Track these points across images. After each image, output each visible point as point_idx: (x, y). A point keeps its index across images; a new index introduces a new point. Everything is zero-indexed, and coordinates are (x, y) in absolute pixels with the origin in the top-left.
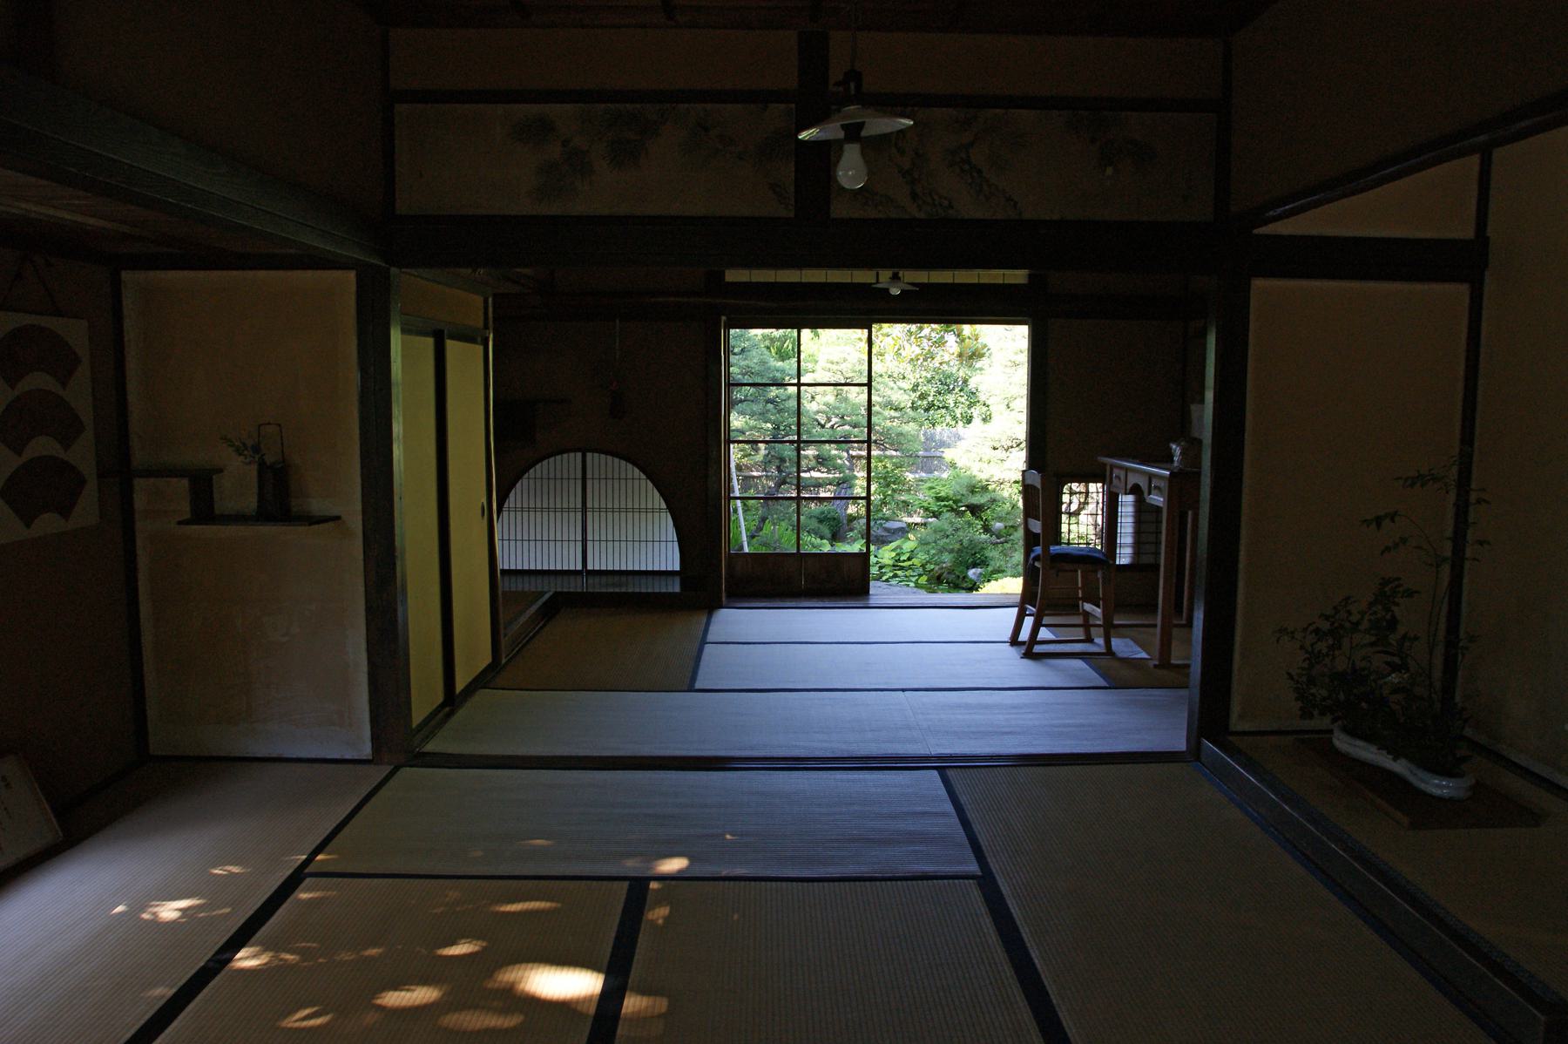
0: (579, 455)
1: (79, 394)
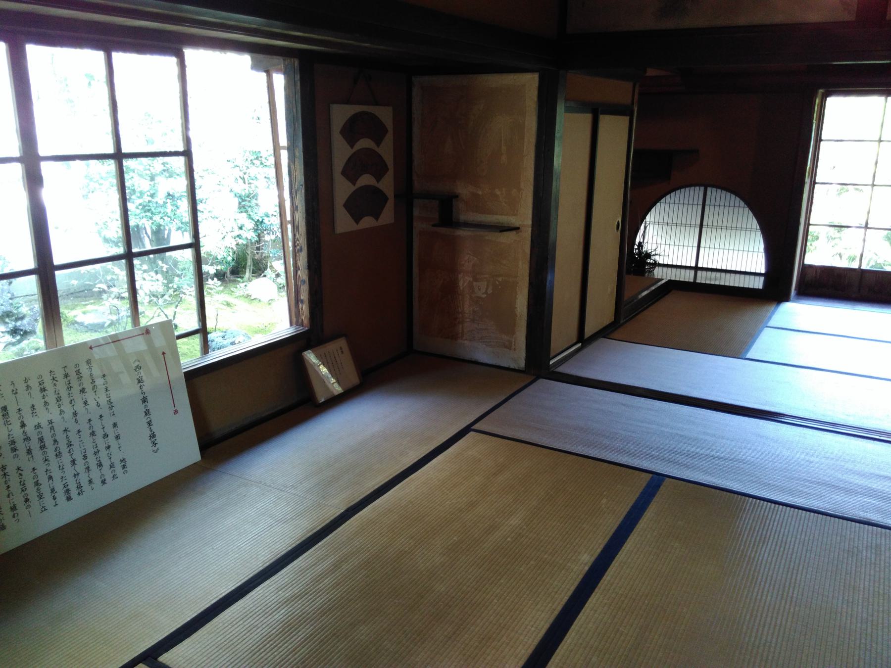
0: (702, 188)
1: (386, 150)
